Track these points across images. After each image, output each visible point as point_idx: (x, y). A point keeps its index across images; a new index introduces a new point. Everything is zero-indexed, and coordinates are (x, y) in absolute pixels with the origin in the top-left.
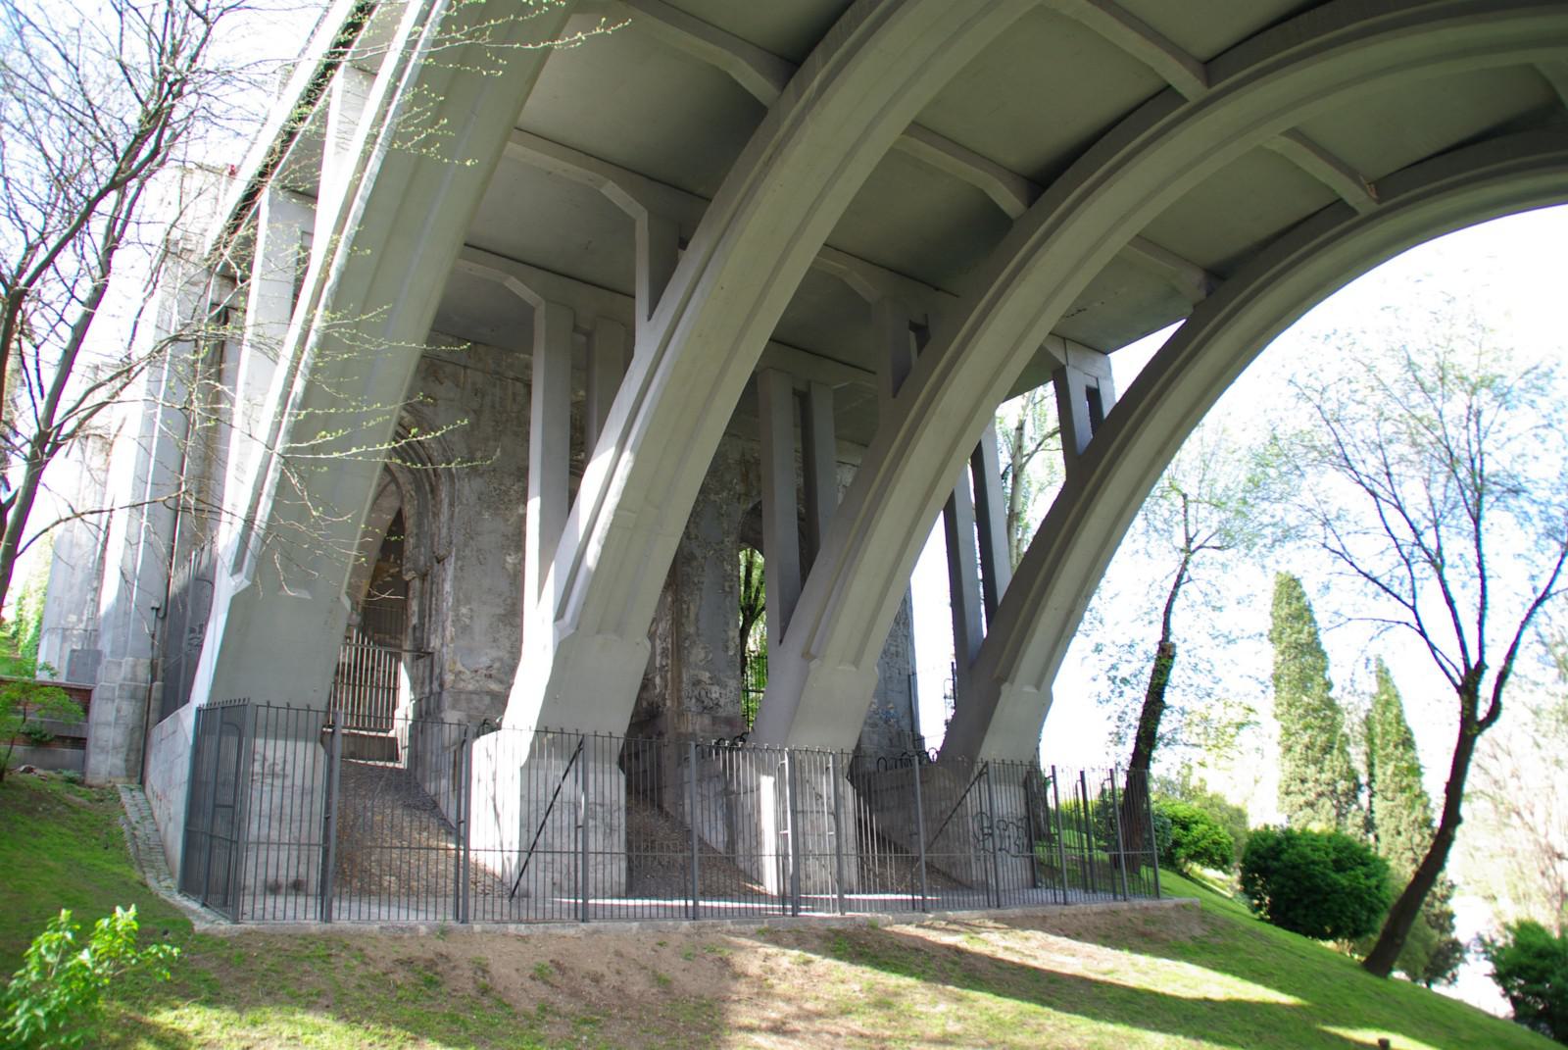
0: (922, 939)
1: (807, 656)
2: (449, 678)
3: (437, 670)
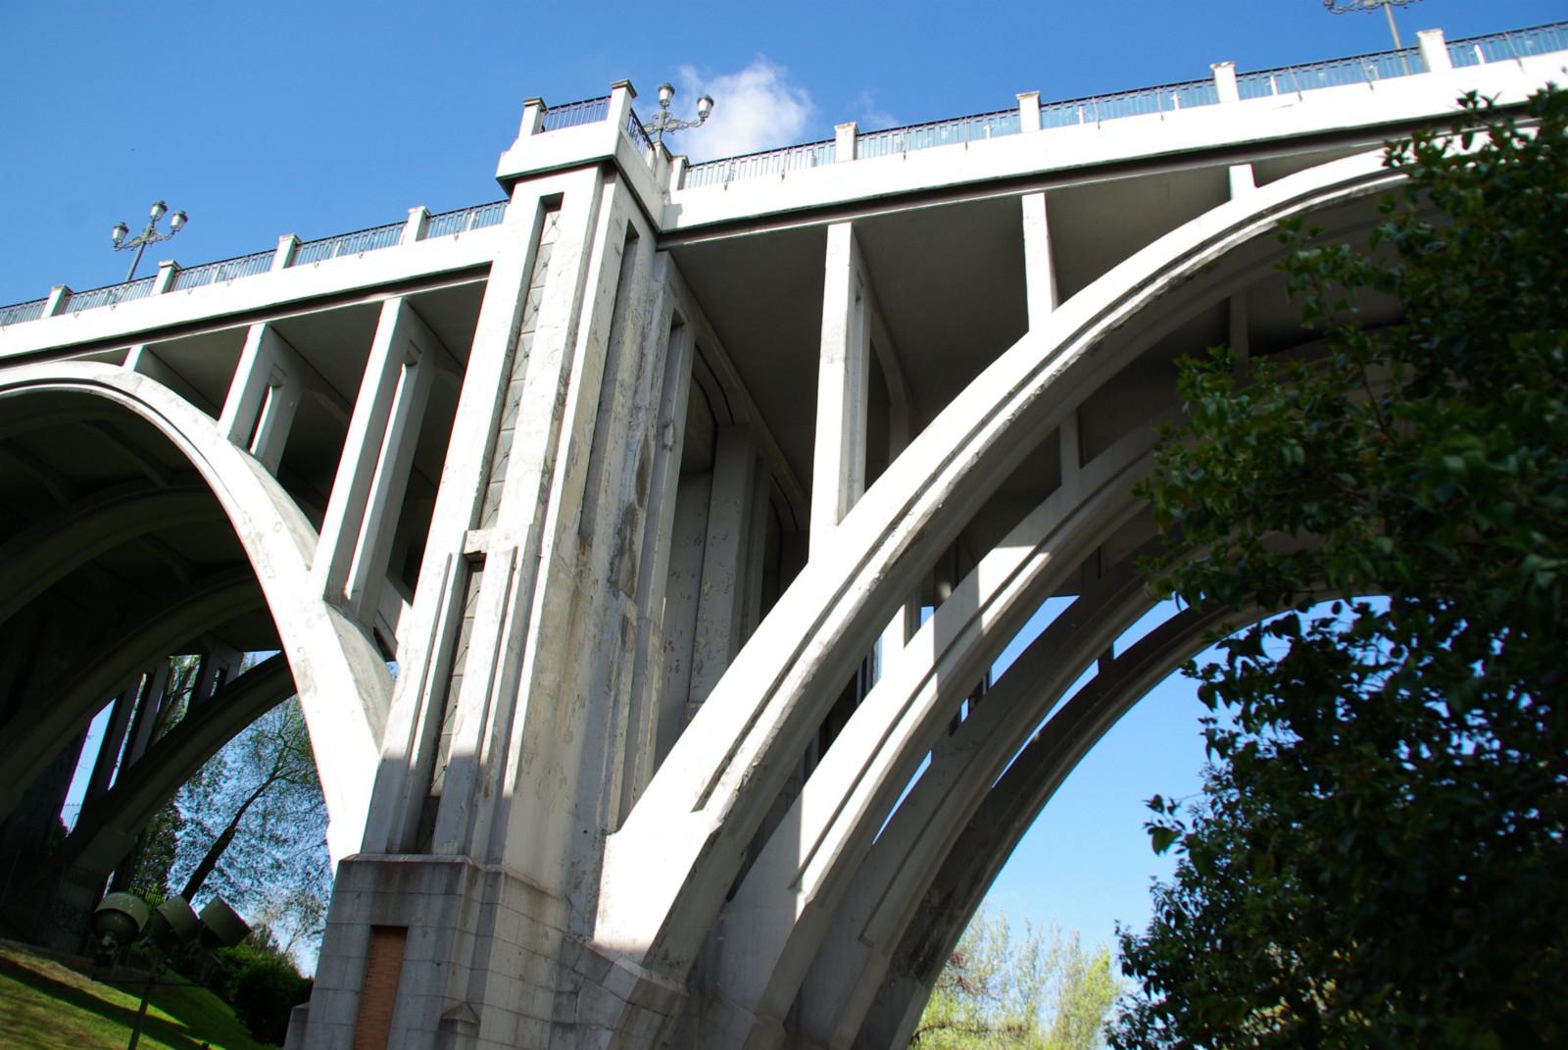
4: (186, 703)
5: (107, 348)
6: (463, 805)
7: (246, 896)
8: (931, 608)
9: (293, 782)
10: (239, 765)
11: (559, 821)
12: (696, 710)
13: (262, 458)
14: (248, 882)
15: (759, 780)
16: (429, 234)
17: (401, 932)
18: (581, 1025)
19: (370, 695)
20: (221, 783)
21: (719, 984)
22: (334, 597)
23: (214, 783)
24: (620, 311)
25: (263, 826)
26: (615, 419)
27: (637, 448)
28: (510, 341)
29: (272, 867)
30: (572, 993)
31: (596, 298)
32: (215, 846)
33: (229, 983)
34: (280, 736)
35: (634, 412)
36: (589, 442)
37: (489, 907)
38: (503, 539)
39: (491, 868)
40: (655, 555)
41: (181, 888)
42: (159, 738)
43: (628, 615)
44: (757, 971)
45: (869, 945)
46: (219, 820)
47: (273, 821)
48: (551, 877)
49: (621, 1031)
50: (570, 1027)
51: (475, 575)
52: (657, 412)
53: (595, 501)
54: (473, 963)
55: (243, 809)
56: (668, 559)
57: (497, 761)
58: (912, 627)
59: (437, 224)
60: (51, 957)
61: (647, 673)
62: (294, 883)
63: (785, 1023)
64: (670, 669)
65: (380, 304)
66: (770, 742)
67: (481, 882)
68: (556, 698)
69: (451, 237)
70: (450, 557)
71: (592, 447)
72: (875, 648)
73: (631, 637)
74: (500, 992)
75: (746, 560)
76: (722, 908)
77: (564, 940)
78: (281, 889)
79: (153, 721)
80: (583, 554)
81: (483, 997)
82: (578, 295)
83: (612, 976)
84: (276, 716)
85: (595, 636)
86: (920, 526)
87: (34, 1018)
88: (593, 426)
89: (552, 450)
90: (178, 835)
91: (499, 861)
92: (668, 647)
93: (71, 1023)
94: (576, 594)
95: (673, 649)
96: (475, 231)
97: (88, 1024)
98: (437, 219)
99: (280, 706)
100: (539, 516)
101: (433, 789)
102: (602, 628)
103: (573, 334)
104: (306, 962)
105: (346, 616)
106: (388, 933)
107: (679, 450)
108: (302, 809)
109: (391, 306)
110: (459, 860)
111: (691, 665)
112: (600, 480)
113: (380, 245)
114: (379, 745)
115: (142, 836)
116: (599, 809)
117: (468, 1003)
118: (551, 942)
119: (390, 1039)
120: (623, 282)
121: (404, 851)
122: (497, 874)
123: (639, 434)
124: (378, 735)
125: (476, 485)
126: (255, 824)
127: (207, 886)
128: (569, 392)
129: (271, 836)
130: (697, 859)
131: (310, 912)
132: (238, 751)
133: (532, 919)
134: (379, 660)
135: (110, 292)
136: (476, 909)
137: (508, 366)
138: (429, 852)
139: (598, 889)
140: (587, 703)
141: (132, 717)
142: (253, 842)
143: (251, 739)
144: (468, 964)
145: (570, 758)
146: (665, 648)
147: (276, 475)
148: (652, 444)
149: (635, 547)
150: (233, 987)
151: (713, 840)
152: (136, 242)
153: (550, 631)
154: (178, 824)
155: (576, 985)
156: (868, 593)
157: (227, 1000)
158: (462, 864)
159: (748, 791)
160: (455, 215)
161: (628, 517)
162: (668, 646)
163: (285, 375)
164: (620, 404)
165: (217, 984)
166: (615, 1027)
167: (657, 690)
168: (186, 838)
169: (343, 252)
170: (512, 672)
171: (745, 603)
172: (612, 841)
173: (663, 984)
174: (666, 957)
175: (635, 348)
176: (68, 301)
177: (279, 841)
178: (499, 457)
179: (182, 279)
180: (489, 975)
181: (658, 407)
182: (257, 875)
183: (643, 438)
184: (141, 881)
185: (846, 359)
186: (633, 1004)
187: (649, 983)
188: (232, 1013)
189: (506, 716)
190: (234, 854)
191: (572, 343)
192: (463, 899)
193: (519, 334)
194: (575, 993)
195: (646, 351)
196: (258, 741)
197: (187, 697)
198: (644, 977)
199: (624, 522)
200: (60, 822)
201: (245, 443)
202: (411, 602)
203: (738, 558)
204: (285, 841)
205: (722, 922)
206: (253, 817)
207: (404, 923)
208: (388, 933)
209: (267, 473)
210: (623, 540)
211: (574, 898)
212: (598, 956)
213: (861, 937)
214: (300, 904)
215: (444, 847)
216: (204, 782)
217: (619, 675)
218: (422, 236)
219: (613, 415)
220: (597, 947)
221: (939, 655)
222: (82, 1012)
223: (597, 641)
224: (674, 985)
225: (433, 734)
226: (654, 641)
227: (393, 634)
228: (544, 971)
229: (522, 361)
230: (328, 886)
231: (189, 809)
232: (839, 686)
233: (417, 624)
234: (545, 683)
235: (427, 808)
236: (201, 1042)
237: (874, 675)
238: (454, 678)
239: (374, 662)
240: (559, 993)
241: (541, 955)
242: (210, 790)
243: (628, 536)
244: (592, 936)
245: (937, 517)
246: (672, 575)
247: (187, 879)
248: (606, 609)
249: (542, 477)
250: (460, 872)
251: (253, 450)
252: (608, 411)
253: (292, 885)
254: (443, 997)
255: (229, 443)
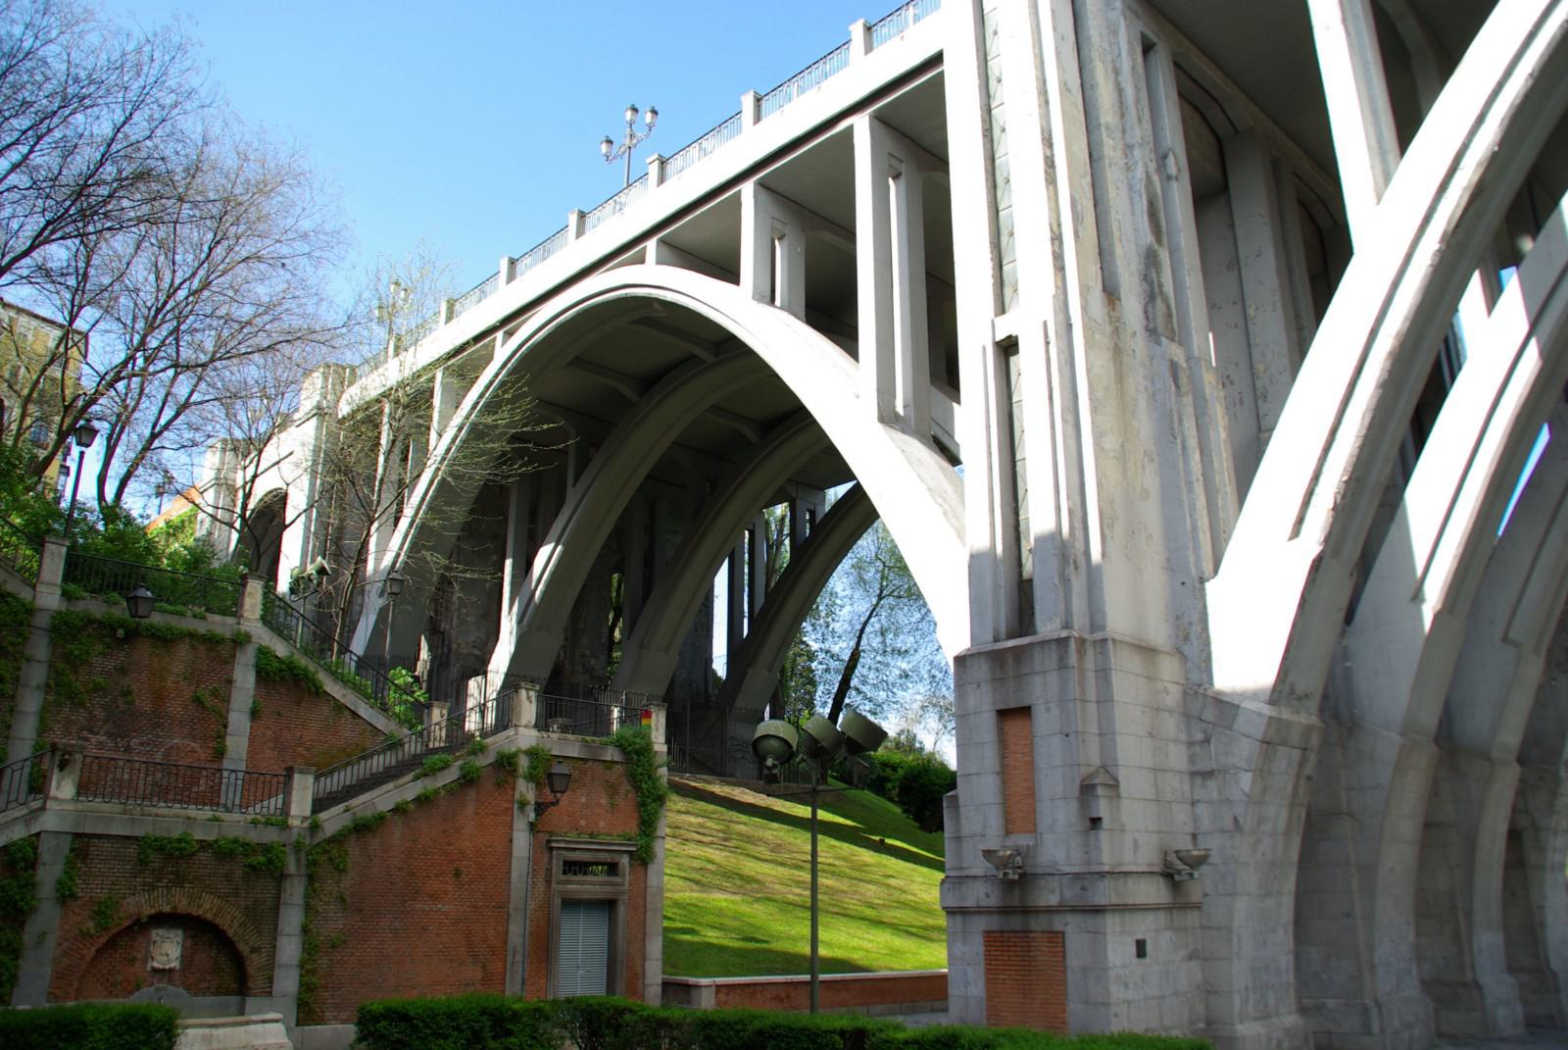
0: (444, 491)
1: (641, 647)
2: (454, 646)
3: (446, 642)
4: (788, 548)
5: (627, 251)
6: (1056, 582)
7: (885, 707)
8: (1513, 269)
9: (899, 597)
10: (848, 592)
11: (1155, 579)
12: (1269, 438)
13: (788, 308)
14: (883, 695)
15: (1353, 494)
16: (875, 45)
17: (1025, 711)
18: (1219, 771)
19: (945, 500)
20: (837, 612)
21: (1355, 711)
22: (888, 417)
23: (830, 613)
24: (1085, 52)
25: (884, 642)
26: (1110, 165)
27: (1141, 187)
28: (983, 121)
29: (901, 677)
30: (1203, 742)
31: (1056, 48)
32: (846, 668)
33: (889, 785)
34: (877, 558)
35: (1128, 152)
36: (1090, 196)
37: (1104, 673)
38: (1029, 319)
39: (1098, 636)
40: (1189, 291)
41: (828, 710)
42: (773, 583)
43: (1176, 359)
44: (1393, 691)
45: (1517, 645)
46: (844, 645)
47: (891, 636)
48: (1158, 633)
49: (1261, 771)
50: (1208, 775)
51: (1013, 360)
52: (1152, 144)
53: (1112, 254)
54: (1100, 729)
55: (862, 631)
56: (1203, 291)
57: (1079, 533)
58: (1493, 292)
59: (881, 31)
60: (739, 784)
61: (1209, 412)
62: (923, 688)
63: (1436, 740)
64: (1232, 405)
65: (850, 129)
66: (1356, 452)
67: (1090, 652)
68: (1122, 457)
69: (897, 39)
70: (984, 348)
71: (1095, 200)
72: (1455, 321)
73: (1184, 381)
74: (1133, 754)
75: (1287, 271)
76: (1343, 634)
77: (1185, 693)
78: (914, 695)
79: (764, 570)
80: (1114, 310)
81: (1116, 759)
82: (1037, 51)
83: (1240, 719)
84: (869, 541)
85: (1146, 389)
86: (1476, 178)
87: (740, 834)
88: (1089, 178)
89: (1054, 215)
90: (814, 665)
91: (1103, 628)
92: (1227, 382)
93: (768, 835)
94: (1117, 351)
95: (1232, 383)
96: (918, 24)
97: (781, 834)
98: (878, 27)
99: (870, 530)
100: (1060, 284)
101: (1024, 573)
102: (1151, 378)
103: (1043, 93)
104: (948, 754)
105: (904, 432)
106: (1015, 714)
107: (1186, 177)
108: (913, 620)
109: (861, 126)
110: (1064, 634)
111: (1255, 395)
112: (1112, 231)
113: (833, 72)
114: (964, 544)
115: (783, 671)
116: (1192, 559)
117: (1103, 767)
118: (1173, 696)
119: (1038, 810)
120: (1079, 23)
121: (1011, 636)
122: (1104, 641)
123: (1140, 173)
124: (960, 534)
125: (990, 272)
126: (876, 642)
127: (848, 705)
128: (1055, 152)
129: (893, 650)
130: (1305, 588)
131: (943, 711)
132: (844, 580)
133: (1149, 678)
134: (946, 465)
135: (615, 201)
136: (1091, 678)
137: (989, 146)
138: (1034, 633)
139: (1208, 637)
140: (1155, 456)
141: (746, 570)
142: (879, 658)
143: (853, 566)
144: (1095, 730)
145: (1151, 515)
146: (1223, 384)
147: (802, 312)
148: (1156, 178)
149: (1165, 289)
150: (894, 788)
151: (1317, 565)
152: (622, 150)
153: (1099, 394)
154: (811, 656)
155: (1206, 735)
156: (1431, 269)
157: (891, 800)
158: (1068, 638)
159: (1343, 509)
160: (894, 17)
161: (1150, 259)
162: (1226, 381)
163: (785, 224)
164: (1111, 148)
165: (879, 786)
166: (1253, 767)
167: (1224, 427)
168: (820, 667)
169: (802, 90)
170: (1072, 443)
171: (1297, 316)
172: (1210, 587)
173: (1295, 718)
174: (1292, 692)
175: (1111, 86)
176: (584, 222)
177: (902, 653)
178: (1004, 239)
179: (670, 168)
180: (1118, 738)
181: (1151, 139)
182: (889, 687)
183: (1144, 176)
184: (794, 711)
185: (1344, 20)
186: (1268, 743)
187: (1280, 720)
188: (898, 810)
189: (1077, 489)
190: (865, 671)
191: (1045, 102)
192: (1076, 671)
193: (990, 111)
194: (1207, 741)
195: (1123, 85)
196: (859, 567)
197: (787, 542)
198: (1274, 714)
199: (1147, 266)
200: (714, 673)
201: (769, 298)
202: (959, 402)
203: (1278, 271)
204: (906, 651)
205: (1346, 648)
206: (872, 636)
207: (1026, 703)
208: (1015, 714)
209: (792, 318)
210: (1151, 284)
211: (1186, 650)
212: (1222, 702)
213: (1505, 639)
214: (935, 705)
215: (1047, 626)
216: (823, 614)
217: (1180, 421)
218: (869, 48)
219: (1107, 161)
220: (1219, 693)
221: (1535, 309)
222: (775, 825)
223: (1150, 392)
224: (1306, 717)
225: (1012, 522)
226: (1209, 380)
227: (952, 437)
228: (1171, 725)
229: (1000, 137)
230: (951, 682)
231: (816, 640)
232: (1424, 376)
233: (972, 418)
234: (1107, 446)
235: (1023, 593)
236: (877, 838)
237: (1462, 358)
238: (1018, 464)
239: (941, 468)
240: (1190, 744)
241: (1166, 710)
242: (830, 620)
243: (1155, 280)
244: (1212, 684)
245: (1495, 164)
246: (1213, 308)
247: (830, 701)
248: (1151, 359)
249: (1053, 244)
250: (1067, 646)
251: (778, 302)
252: (1101, 158)
253: (922, 690)
254: (1079, 765)
255: (756, 303)
